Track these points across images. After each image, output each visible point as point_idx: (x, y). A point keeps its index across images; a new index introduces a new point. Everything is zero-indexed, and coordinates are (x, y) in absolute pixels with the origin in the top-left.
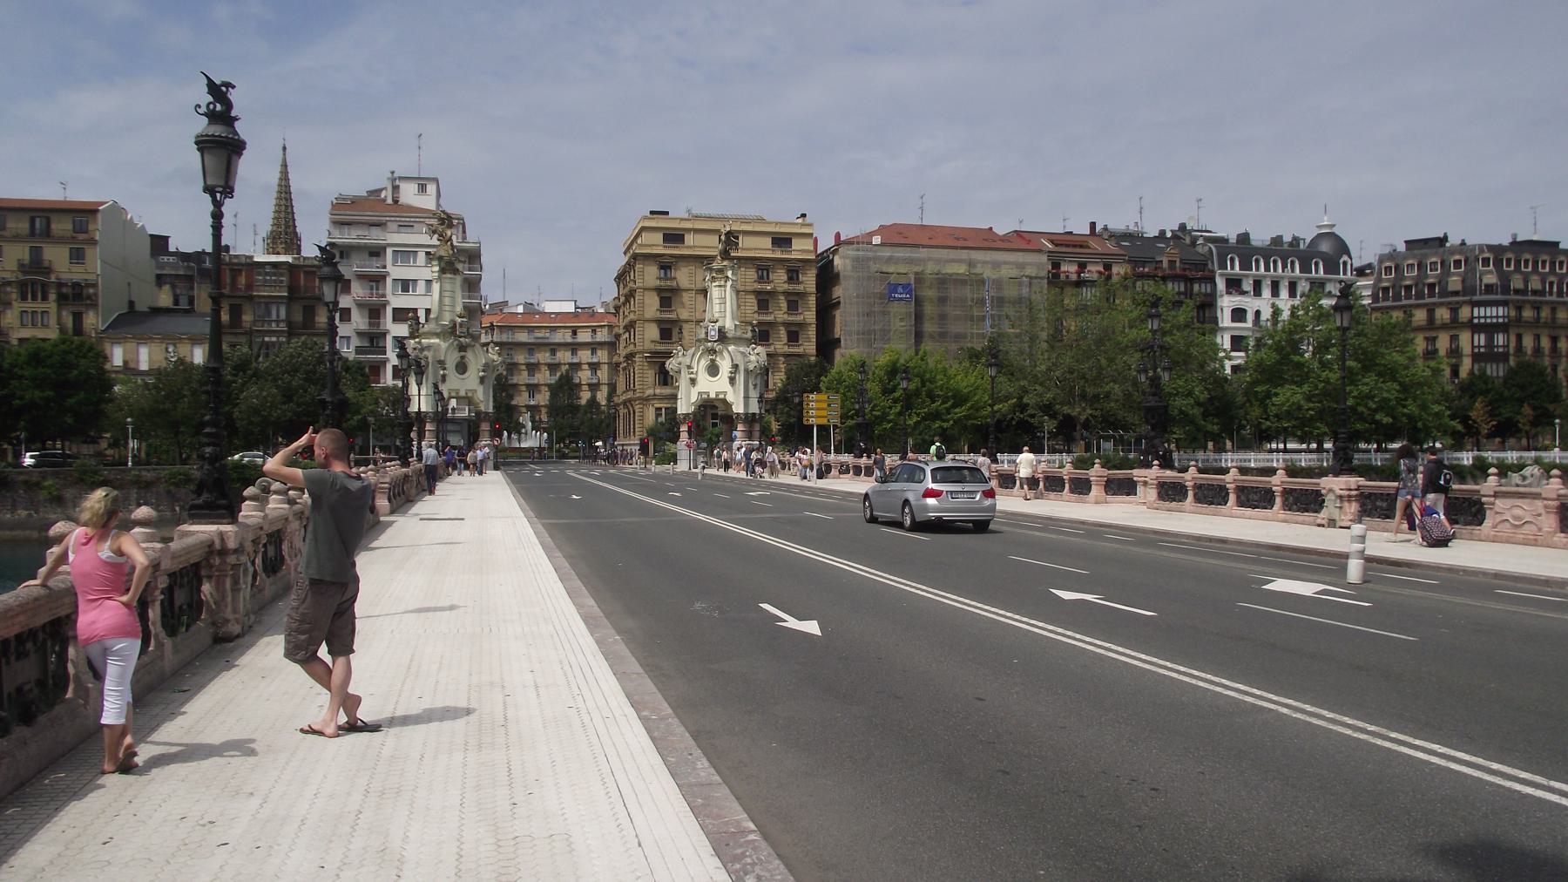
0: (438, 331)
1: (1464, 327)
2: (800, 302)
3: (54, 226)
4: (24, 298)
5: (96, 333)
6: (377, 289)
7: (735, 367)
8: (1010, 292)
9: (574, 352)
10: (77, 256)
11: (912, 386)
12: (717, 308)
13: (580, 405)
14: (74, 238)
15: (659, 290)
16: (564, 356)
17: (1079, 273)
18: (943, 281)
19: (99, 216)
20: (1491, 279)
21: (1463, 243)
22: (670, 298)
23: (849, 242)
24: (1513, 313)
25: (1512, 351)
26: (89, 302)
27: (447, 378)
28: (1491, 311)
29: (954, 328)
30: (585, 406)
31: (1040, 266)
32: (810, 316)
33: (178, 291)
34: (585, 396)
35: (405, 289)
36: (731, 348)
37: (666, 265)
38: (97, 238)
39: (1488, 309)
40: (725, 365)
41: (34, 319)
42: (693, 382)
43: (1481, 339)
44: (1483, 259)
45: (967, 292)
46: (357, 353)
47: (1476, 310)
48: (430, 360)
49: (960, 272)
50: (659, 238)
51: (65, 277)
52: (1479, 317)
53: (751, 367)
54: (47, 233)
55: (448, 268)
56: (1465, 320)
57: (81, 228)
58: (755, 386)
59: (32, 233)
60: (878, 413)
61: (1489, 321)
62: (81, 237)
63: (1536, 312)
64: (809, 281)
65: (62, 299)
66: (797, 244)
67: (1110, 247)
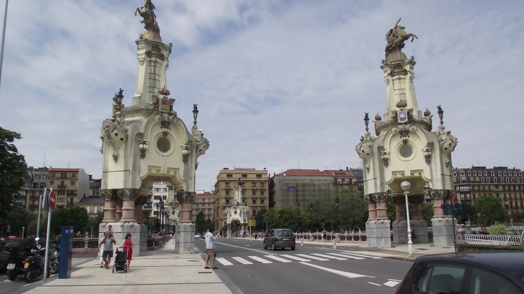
0: (168, 204)
1: (458, 192)
2: (264, 192)
3: (67, 175)
4: (59, 194)
5: (76, 203)
6: (150, 191)
7: (241, 212)
8: (323, 188)
9: (204, 205)
10: (73, 183)
11: (287, 216)
12: (237, 197)
13: (205, 221)
14: (72, 178)
15: (226, 190)
16: (201, 206)
17: (342, 182)
18: (304, 185)
19: (79, 172)
20: (464, 178)
21: (457, 168)
22: (229, 192)
23: (277, 175)
24: (471, 188)
25: (472, 198)
26: (75, 195)
27: (146, 153)
28: (465, 188)
29: (307, 198)
30: (207, 221)
31: (331, 180)
32: (266, 194)
33: (94, 190)
34: (207, 218)
35: (158, 191)
36: (240, 207)
37: (227, 183)
38: (78, 178)
39: (464, 187)
40: (238, 211)
41: (61, 200)
42: (231, 216)
43: (463, 196)
44: (462, 173)
45: (310, 188)
46: (144, 208)
47: (460, 187)
48: (129, 133)
49: (309, 182)
50: (225, 176)
51: (69, 188)
52: (462, 190)
53: (245, 212)
54: (65, 178)
55: (154, 52)
56: (458, 190)
57: (74, 176)
58: (246, 216)
59: (62, 178)
60: (278, 223)
61: (464, 190)
62: (74, 178)
63: (479, 187)
64: (267, 186)
65: (68, 194)
66: (263, 176)
67: (352, 174)
